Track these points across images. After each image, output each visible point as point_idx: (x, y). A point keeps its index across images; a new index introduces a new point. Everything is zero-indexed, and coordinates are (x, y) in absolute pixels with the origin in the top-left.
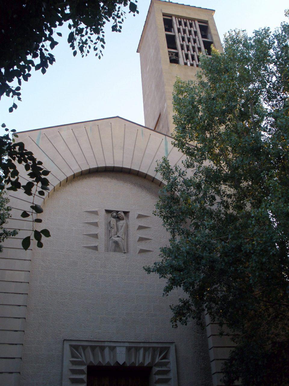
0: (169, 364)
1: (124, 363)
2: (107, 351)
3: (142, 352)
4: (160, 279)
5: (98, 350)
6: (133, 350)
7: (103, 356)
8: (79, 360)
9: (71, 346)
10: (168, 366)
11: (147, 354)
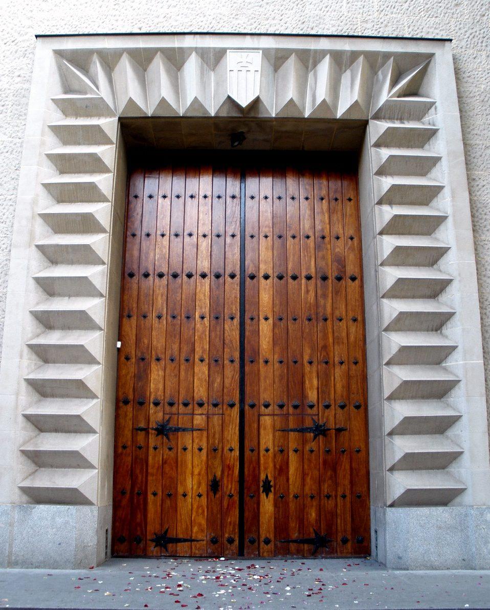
0: (433, 108)
1: (257, 102)
2: (192, 66)
3: (325, 68)
4: (453, 38)
5: (158, 66)
6: (291, 64)
7: (177, 86)
8: (88, 96)
9: (59, 53)
11: (346, 78)
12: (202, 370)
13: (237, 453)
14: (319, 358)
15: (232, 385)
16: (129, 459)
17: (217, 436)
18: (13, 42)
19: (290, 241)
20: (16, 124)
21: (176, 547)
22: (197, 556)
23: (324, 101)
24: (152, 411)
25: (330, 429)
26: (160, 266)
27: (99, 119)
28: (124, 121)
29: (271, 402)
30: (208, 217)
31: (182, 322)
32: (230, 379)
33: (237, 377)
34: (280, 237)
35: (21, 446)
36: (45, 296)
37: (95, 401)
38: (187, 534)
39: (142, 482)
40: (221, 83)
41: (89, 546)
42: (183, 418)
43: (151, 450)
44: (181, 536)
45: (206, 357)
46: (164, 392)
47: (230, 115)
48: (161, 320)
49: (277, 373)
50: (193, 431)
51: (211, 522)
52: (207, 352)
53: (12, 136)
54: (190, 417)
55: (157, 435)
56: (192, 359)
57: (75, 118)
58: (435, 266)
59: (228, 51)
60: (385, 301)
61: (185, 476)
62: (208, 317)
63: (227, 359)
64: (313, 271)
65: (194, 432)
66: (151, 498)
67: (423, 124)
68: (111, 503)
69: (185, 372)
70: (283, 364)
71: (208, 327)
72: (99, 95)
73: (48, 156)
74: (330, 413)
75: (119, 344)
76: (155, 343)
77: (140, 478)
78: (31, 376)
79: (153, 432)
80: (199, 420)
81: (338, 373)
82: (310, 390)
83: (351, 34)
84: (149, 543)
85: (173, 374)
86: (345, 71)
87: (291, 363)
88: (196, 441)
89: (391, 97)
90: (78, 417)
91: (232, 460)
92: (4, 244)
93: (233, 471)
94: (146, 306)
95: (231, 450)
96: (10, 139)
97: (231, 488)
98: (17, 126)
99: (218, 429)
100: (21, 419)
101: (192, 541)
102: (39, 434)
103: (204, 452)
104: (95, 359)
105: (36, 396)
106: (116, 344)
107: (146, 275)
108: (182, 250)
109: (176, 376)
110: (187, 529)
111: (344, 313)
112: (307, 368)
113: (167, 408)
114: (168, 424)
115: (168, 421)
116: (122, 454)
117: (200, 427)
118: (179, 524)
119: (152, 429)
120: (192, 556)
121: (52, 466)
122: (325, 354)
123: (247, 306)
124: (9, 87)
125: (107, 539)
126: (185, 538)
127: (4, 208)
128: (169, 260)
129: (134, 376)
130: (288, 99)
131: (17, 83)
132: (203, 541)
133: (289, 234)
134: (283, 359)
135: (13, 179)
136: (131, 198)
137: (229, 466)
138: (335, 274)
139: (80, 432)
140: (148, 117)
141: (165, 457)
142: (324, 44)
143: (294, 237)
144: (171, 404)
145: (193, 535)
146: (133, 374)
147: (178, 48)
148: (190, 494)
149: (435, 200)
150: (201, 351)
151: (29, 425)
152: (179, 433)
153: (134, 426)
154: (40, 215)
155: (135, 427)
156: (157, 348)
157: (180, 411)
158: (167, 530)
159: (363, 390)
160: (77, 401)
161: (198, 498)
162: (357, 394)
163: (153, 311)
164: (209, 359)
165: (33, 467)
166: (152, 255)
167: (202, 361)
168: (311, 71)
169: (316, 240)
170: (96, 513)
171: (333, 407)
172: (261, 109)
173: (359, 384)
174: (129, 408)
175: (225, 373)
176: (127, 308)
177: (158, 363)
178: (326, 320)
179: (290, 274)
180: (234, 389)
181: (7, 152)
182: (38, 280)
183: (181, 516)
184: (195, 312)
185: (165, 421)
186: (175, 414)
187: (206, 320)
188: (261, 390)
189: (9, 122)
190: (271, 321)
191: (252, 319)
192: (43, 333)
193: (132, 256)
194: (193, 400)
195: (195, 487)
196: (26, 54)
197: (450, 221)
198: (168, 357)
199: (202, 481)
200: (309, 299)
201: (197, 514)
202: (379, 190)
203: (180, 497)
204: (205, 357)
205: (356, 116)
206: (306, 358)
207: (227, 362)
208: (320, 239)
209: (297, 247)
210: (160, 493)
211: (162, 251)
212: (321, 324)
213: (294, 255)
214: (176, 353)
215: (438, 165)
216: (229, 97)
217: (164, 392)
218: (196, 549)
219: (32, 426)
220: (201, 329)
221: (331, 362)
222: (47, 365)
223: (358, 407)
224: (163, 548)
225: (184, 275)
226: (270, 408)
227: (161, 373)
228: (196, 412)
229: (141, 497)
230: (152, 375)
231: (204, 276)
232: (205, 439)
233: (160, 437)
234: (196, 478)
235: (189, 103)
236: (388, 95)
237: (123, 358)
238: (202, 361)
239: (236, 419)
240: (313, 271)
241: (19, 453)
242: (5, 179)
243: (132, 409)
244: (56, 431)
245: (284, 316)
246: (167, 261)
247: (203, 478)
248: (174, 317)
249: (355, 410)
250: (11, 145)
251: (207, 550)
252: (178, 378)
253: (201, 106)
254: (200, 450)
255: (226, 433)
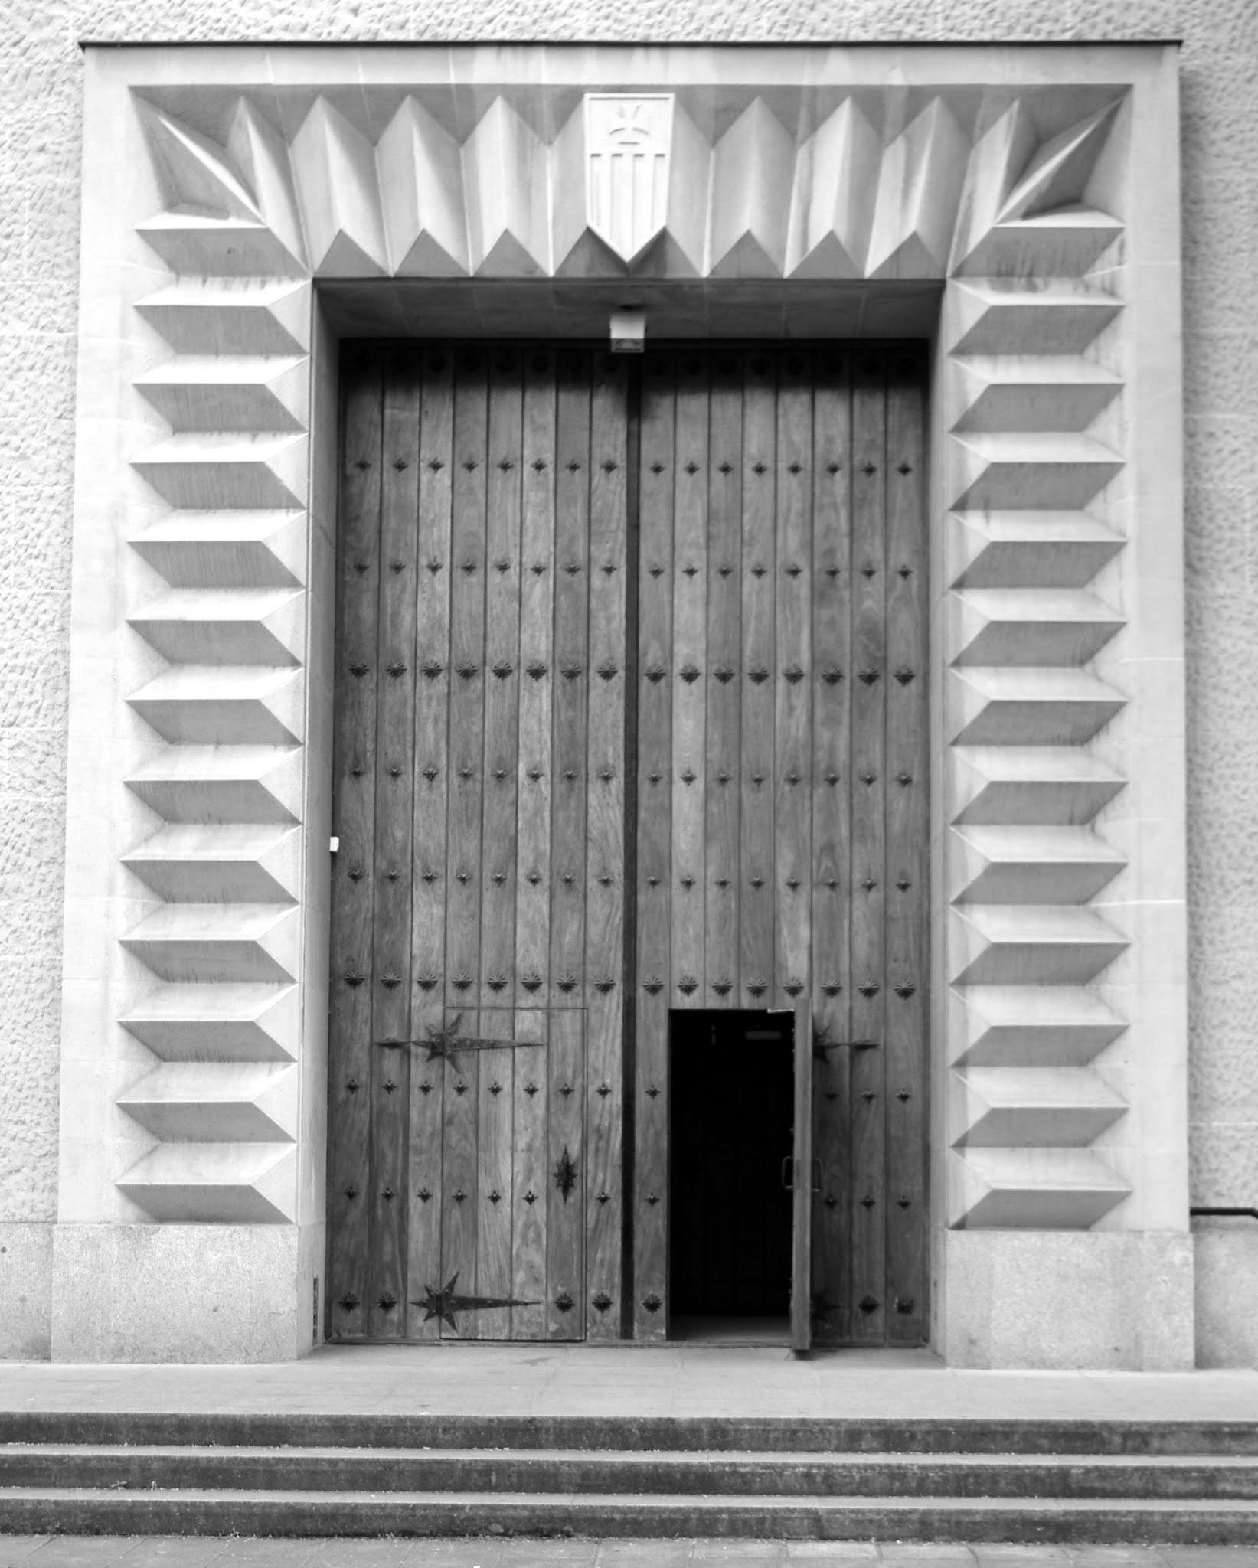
0: (1112, 252)
8: (233, 223)
9: (147, 97)
10: (1099, 273)
12: (533, 903)
13: (616, 1099)
14: (815, 874)
15: (607, 940)
16: (365, 1115)
17: (570, 1059)
18: (15, 44)
19: (750, 582)
20: (47, 291)
21: (476, 1319)
22: (525, 1338)
23: (831, 235)
24: (415, 1003)
25: (837, 1045)
26: (430, 647)
27: (263, 284)
28: (324, 285)
29: (699, 981)
30: (547, 522)
31: (486, 787)
32: (601, 924)
33: (618, 919)
34: (725, 573)
35: (118, 1097)
36: (157, 744)
37: (288, 989)
38: (501, 1287)
39: (395, 1169)
40: (571, 185)
41: (279, 1314)
42: (490, 1018)
43: (416, 1095)
44: (486, 1293)
45: (544, 871)
46: (445, 956)
47: (594, 275)
48: (434, 783)
49: (713, 911)
50: (513, 1048)
51: (556, 1261)
52: (547, 859)
53: (41, 325)
54: (506, 1014)
55: (430, 1058)
56: (510, 876)
57: (200, 280)
58: (1088, 667)
59: (587, 96)
60: (959, 752)
61: (496, 1153)
62: (549, 773)
63: (593, 876)
64: (804, 662)
65: (517, 1050)
66: (415, 1203)
67: (1087, 288)
68: (323, 1219)
69: (494, 909)
70: (728, 887)
71: (549, 800)
72: (258, 221)
73: (145, 390)
74: (838, 1007)
75: (334, 844)
76: (420, 837)
77: (390, 1159)
78: (137, 936)
79: (420, 1050)
80: (528, 1023)
81: (862, 907)
82: (792, 950)
83: (909, 33)
84: (412, 1308)
85: (465, 914)
86: (893, 139)
87: (747, 887)
88: (522, 1071)
89: (1006, 219)
90: (251, 1026)
91: (606, 1115)
92: (45, 612)
93: (608, 1142)
94: (398, 748)
95: (604, 1092)
96: (37, 333)
97: (604, 1182)
98: (50, 296)
99: (573, 1042)
100: (116, 1034)
101: (512, 1303)
102: (158, 1067)
103: (540, 1096)
104: (284, 891)
105: (149, 980)
106: (328, 843)
107: (397, 673)
108: (482, 608)
109: (473, 916)
110: (501, 1276)
111: (878, 766)
112: (786, 897)
113: (453, 994)
114: (456, 1031)
115: (457, 1023)
116: (346, 1102)
117: (531, 1039)
118: (481, 1266)
119: (416, 1043)
120: (514, 1338)
121: (190, 1139)
122: (830, 864)
123: (642, 749)
124: (19, 183)
125: (315, 1302)
126: (497, 1297)
127: (38, 520)
128: (450, 631)
129: (373, 919)
130: (740, 233)
131: (39, 171)
132: (538, 1303)
133: (748, 564)
134: (727, 877)
135: (54, 442)
136: (351, 469)
137: (598, 1130)
138: (863, 666)
139: (254, 1059)
140: (388, 279)
141: (448, 1109)
142: (838, 70)
143: (759, 573)
144: (463, 986)
145: (516, 1291)
146: (370, 914)
147: (458, 86)
148: (508, 1196)
149: (1100, 496)
150: (531, 859)
151: (135, 1046)
152: (482, 1052)
153: (374, 1036)
154: (137, 546)
155: (377, 1039)
156: (427, 849)
157: (485, 1002)
158: (455, 1278)
159: (921, 953)
160: (245, 990)
161: (526, 1204)
162: (906, 961)
163: (414, 759)
164: (551, 877)
165: (147, 1141)
166: (407, 617)
167: (534, 881)
168: (804, 142)
169: (816, 577)
170: (294, 1241)
171: (845, 992)
172: (671, 257)
173: (911, 938)
174: (362, 994)
175: (589, 910)
176: (351, 754)
177: (430, 887)
178: (833, 781)
179: (748, 666)
180: (610, 949)
181: (32, 368)
182: (140, 708)
183: (486, 1247)
184: (518, 761)
185: (448, 1025)
186: (472, 1008)
187: (544, 784)
188: (677, 949)
189: (28, 283)
190: (699, 784)
191: (655, 780)
192: (158, 831)
193: (358, 620)
194: (514, 975)
195: (519, 1179)
196: (53, 84)
197: (1129, 556)
198: (452, 873)
199: (535, 1165)
200: (793, 730)
201: (525, 1242)
202: (961, 473)
203: (484, 1203)
204: (541, 871)
205: (913, 271)
206: (784, 874)
207: (593, 883)
208: (824, 577)
209: (767, 600)
210: (437, 1194)
211: (434, 610)
212: (821, 790)
213: (759, 618)
214: (473, 862)
215: (1114, 405)
216: (589, 233)
217: (445, 956)
218: (526, 1320)
219: (142, 1047)
220: (530, 805)
221: (844, 885)
222: (171, 905)
223: (906, 993)
224: (444, 1321)
225: (488, 669)
226: (696, 993)
227: (438, 911)
228: (521, 1003)
229: (394, 1203)
230: (416, 914)
231: (536, 673)
232: (541, 1067)
233: (436, 1062)
234: (521, 1158)
235: (487, 250)
236: (996, 217)
237: (344, 878)
238: (534, 881)
239: (616, 1019)
240: (804, 662)
241: (116, 1111)
242: (34, 443)
243: (368, 997)
244: (198, 1057)
245: (732, 772)
246: (447, 634)
247: (536, 1158)
248: (466, 776)
249: (900, 1001)
250: (42, 347)
251: (547, 1325)
252: (477, 922)
253: (522, 253)
254: (531, 1091)
255: (592, 1053)
